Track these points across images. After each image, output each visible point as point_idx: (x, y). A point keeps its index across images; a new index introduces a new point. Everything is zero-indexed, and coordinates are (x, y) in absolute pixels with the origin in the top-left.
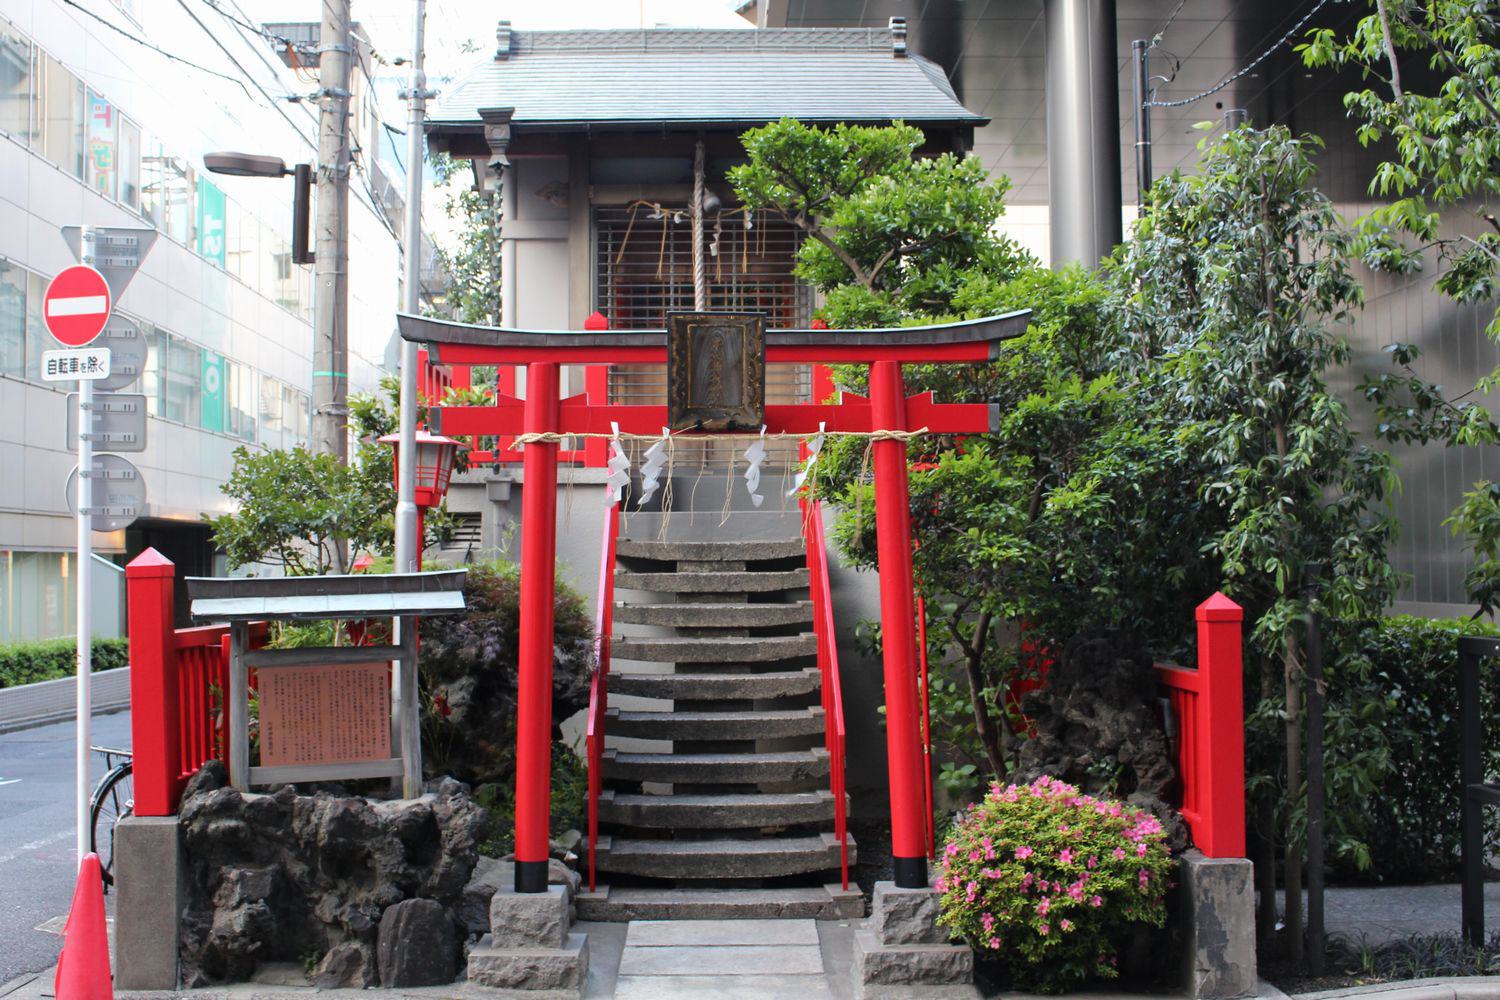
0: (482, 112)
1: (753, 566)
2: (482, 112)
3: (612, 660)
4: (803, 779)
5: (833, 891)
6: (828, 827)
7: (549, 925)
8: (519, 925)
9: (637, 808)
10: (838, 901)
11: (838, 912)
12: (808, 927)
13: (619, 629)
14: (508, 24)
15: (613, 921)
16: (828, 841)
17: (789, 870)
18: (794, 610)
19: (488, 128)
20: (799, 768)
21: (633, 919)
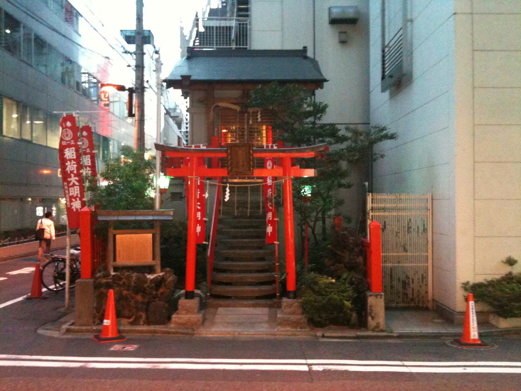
2: (182, 76)
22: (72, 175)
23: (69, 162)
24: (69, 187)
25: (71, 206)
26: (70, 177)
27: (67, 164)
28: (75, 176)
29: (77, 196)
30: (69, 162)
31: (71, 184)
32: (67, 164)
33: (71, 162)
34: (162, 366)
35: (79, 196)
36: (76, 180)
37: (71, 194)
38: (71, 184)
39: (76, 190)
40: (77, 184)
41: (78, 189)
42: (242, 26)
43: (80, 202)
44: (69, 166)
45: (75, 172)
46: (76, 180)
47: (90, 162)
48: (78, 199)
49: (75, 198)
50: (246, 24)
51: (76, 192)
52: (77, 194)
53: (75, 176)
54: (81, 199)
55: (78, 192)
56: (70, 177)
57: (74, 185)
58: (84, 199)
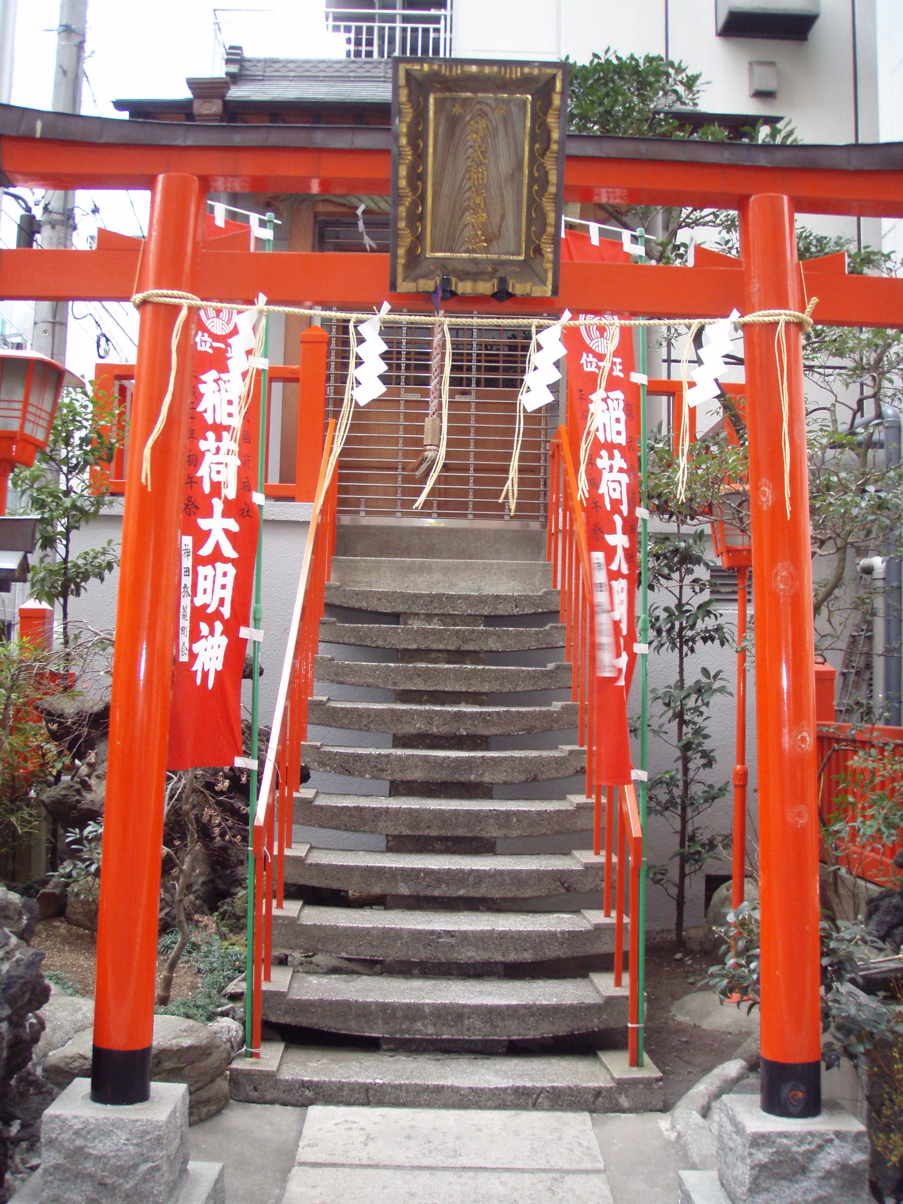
0: (193, 84)
1: (492, 620)
2: (193, 84)
3: (281, 384)
4: (563, 893)
5: (615, 1066)
6: (603, 963)
7: (144, 1167)
8: (89, 1166)
9: (415, 668)
10: (623, 1085)
11: (624, 1102)
12: (577, 1124)
13: (316, 736)
14: (240, 48)
15: (285, 1104)
16: (605, 985)
17: (546, 1030)
18: (544, 674)
19: (196, 104)
20: (561, 877)
21: (312, 1103)
22: (218, 505)
23: (211, 435)
24: (199, 561)
25: (193, 657)
26: (209, 514)
27: (203, 445)
28: (225, 514)
29: (218, 615)
30: (211, 435)
31: (206, 550)
32: (203, 445)
33: (219, 439)
34: (790, 283)
35: (226, 612)
36: (227, 532)
37: (198, 602)
38: (206, 550)
39: (220, 580)
40: (229, 551)
41: (230, 581)
42: (432, 35)
43: (224, 641)
44: (208, 459)
45: (230, 492)
46: (227, 532)
47: (622, 427)
48: (219, 626)
49: (211, 618)
50: (437, 30)
51: (219, 593)
52: (222, 601)
53: (225, 514)
54: (231, 630)
55: (228, 594)
56: (209, 514)
57: (217, 556)
58: (244, 633)
